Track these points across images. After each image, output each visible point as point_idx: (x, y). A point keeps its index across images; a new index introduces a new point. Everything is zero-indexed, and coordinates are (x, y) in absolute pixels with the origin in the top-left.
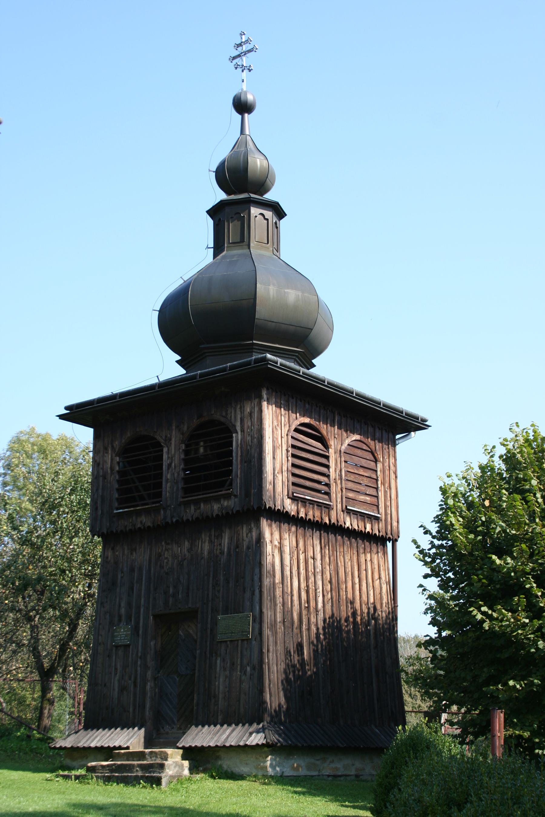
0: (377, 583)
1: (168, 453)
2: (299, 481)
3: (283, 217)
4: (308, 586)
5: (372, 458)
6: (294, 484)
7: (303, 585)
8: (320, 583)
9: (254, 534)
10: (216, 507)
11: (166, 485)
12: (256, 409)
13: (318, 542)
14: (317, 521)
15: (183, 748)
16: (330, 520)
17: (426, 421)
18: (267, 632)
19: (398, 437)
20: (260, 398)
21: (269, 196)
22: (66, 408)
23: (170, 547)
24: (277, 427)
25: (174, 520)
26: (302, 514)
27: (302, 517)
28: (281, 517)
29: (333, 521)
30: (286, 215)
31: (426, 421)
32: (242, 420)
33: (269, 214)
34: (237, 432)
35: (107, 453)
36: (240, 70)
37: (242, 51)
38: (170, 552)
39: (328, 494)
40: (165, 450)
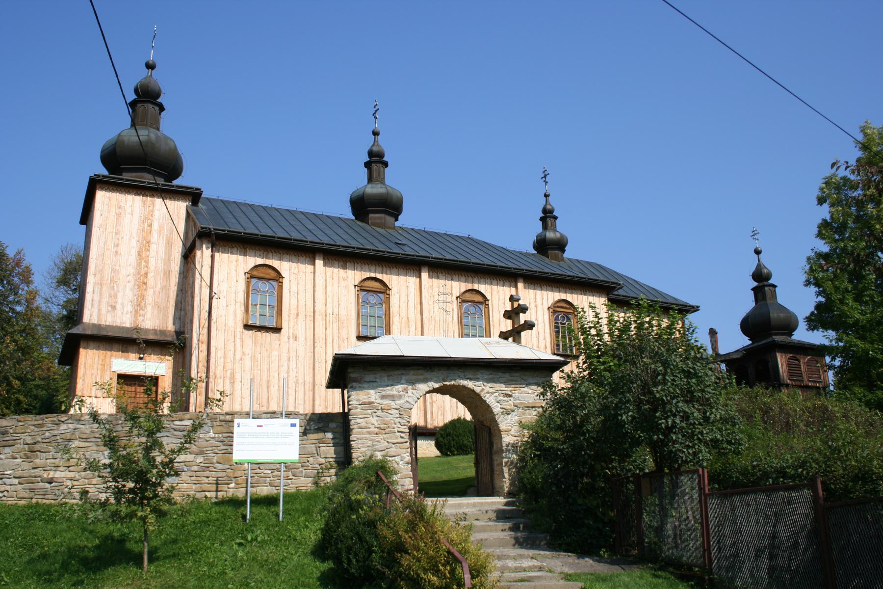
2: (791, 375)
21: (159, 100)
24: (782, 360)
33: (157, 108)
37: (754, 234)
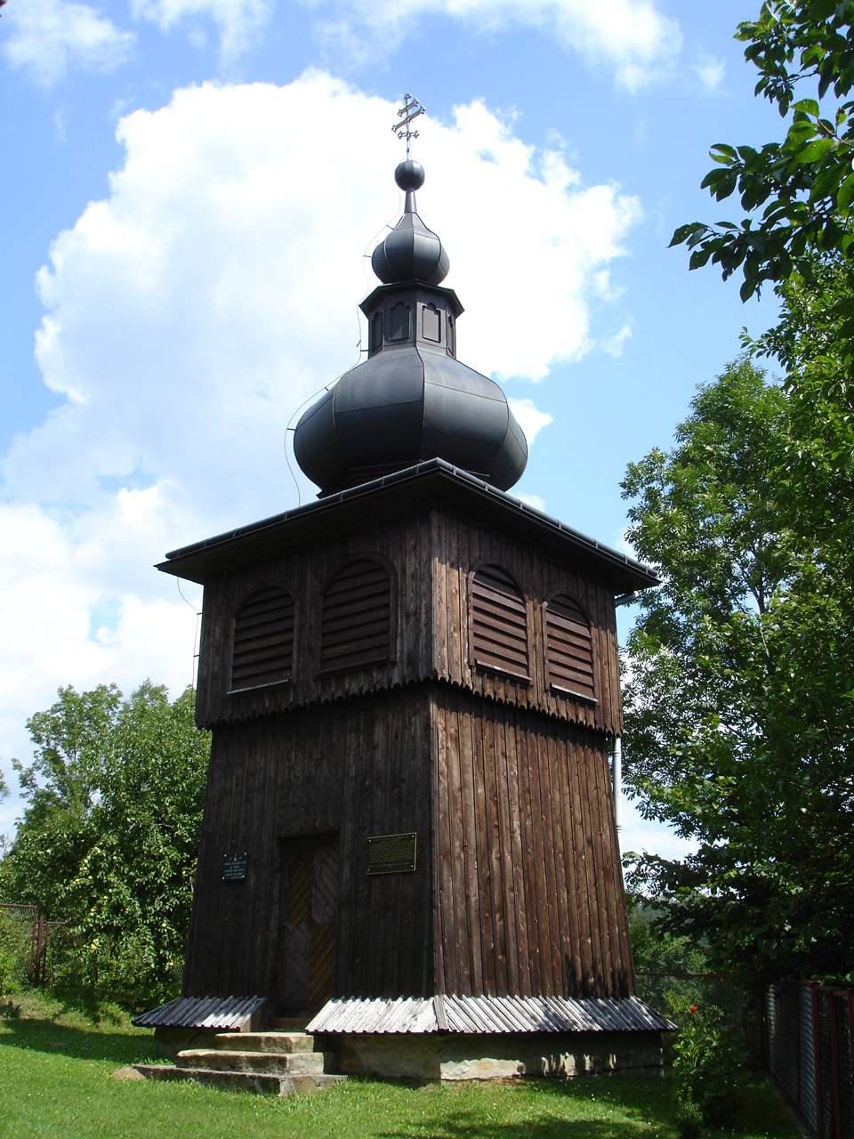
3: (460, 313)
6: (476, 648)
7: (359, 620)
14: (511, 702)
15: (316, 1034)
16: (528, 703)
22: (167, 556)
25: (308, 701)
26: (489, 692)
28: (456, 697)
30: (463, 310)
34: (396, 575)
36: (404, 139)
39: (526, 667)
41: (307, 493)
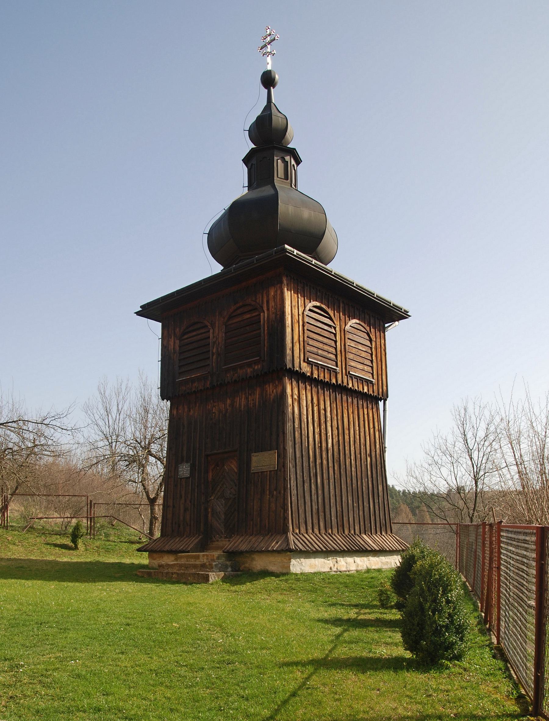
0: (372, 431)
1: (213, 333)
4: (320, 431)
5: (368, 338)
8: (329, 429)
9: (280, 389)
10: (249, 370)
11: (213, 357)
12: (279, 292)
13: (328, 398)
16: (337, 381)
17: (408, 312)
18: (290, 465)
19: (386, 325)
20: (281, 282)
22: (141, 307)
23: (215, 404)
24: (295, 306)
26: (315, 376)
27: (315, 378)
28: (300, 377)
29: (340, 382)
31: (408, 312)
32: (268, 302)
34: (264, 312)
35: (171, 338)
38: (217, 407)
40: (211, 331)
41: (218, 268)
